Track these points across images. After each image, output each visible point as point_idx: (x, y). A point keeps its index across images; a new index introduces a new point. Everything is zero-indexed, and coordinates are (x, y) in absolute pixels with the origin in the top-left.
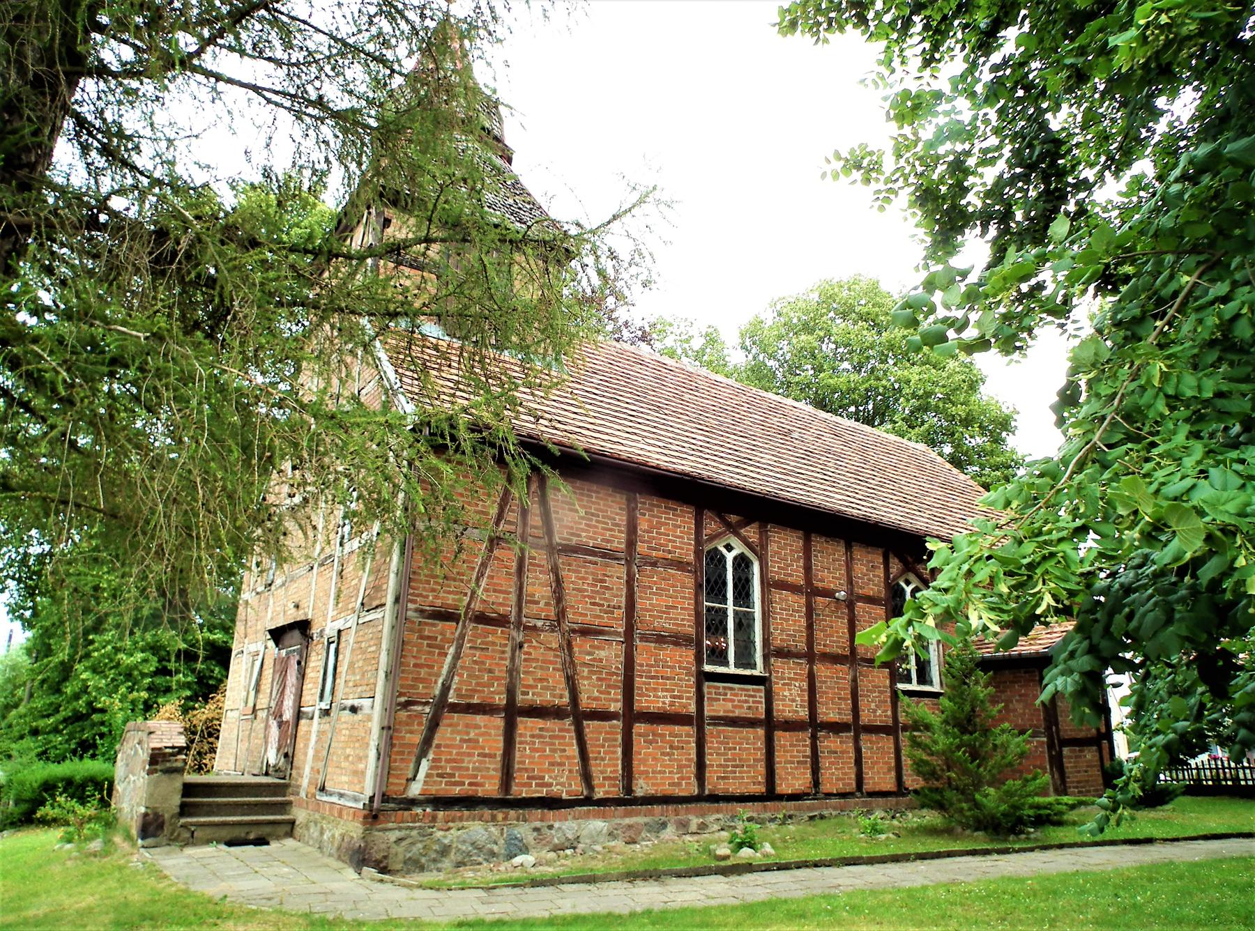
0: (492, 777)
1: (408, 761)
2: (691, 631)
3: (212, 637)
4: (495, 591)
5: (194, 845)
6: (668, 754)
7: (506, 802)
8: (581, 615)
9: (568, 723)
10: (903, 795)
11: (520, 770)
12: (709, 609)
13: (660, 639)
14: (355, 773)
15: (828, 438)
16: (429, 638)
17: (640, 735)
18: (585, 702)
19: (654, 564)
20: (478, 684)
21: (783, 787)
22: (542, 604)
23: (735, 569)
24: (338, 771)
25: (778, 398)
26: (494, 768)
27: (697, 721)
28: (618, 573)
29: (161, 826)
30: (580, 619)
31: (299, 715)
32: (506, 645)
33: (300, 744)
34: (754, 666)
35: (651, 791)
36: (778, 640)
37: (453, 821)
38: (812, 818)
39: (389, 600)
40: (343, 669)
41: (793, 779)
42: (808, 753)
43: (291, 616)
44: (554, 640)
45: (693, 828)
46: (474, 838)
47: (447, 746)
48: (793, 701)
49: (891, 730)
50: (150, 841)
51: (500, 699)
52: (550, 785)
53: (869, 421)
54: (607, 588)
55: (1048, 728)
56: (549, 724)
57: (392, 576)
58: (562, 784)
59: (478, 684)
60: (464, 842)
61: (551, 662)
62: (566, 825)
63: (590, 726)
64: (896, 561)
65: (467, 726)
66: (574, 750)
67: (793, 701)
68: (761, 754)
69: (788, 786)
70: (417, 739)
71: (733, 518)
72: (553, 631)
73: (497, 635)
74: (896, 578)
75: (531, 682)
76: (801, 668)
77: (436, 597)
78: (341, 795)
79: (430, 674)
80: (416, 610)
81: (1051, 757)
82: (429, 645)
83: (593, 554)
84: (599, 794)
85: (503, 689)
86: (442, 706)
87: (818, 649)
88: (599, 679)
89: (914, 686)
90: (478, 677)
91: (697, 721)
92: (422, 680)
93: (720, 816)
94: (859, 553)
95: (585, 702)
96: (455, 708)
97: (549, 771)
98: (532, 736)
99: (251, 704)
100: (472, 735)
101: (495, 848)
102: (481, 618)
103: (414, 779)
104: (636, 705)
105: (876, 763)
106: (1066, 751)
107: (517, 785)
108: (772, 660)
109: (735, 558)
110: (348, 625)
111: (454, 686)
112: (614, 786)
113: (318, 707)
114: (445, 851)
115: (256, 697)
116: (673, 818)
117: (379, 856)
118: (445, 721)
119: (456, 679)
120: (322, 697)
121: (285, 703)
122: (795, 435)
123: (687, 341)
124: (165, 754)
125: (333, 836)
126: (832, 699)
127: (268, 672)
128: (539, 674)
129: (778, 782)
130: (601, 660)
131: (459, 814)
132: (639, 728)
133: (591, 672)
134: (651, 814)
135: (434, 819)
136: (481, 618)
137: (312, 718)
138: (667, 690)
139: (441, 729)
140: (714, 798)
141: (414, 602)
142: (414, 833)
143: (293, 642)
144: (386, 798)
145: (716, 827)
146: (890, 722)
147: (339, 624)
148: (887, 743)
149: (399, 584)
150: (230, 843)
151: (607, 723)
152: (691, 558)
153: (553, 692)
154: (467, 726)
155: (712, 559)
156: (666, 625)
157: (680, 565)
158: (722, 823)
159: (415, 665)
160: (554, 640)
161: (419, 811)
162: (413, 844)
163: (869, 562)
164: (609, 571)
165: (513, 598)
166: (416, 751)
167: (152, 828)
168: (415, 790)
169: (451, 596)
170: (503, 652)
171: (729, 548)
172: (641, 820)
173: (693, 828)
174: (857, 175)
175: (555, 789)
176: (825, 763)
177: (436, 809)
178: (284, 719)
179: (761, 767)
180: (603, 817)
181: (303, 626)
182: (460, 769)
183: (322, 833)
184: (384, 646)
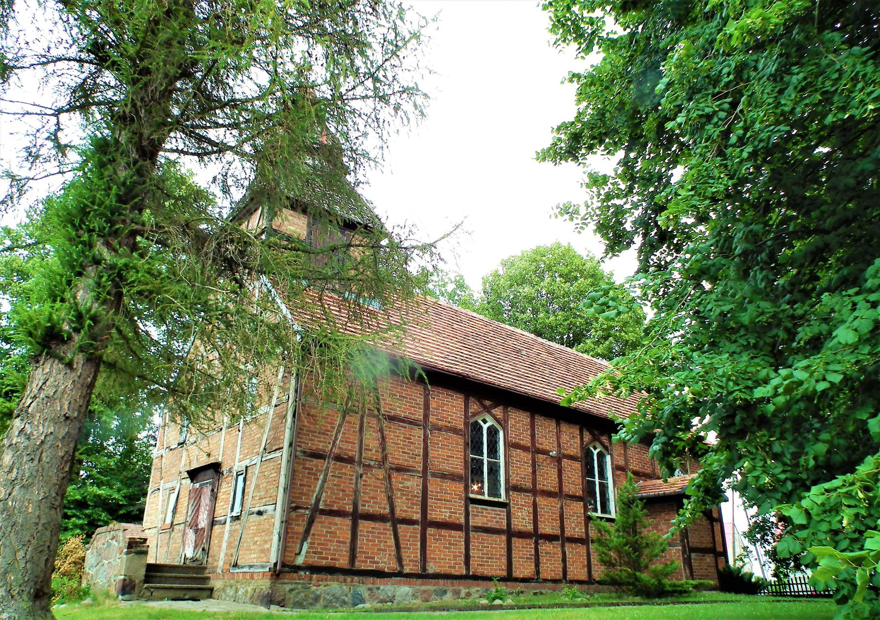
0: (344, 556)
1: (296, 543)
2: (462, 472)
3: (100, 492)
4: (347, 442)
5: (152, 600)
6: (447, 548)
7: (351, 572)
8: (397, 459)
9: (388, 524)
10: (592, 584)
11: (360, 552)
12: (473, 459)
13: (443, 476)
14: (263, 551)
15: (544, 355)
16: (309, 469)
17: (431, 535)
18: (399, 513)
19: (440, 429)
20: (336, 498)
21: (517, 573)
22: (374, 451)
23: (488, 435)
24: (248, 552)
25: (512, 328)
26: (345, 550)
27: (465, 528)
28: (418, 433)
29: (133, 588)
30: (396, 461)
31: (213, 523)
32: (352, 475)
33: (214, 541)
34: (499, 496)
35: (438, 570)
36: (513, 481)
37: (322, 581)
38: (535, 594)
39: (286, 445)
40: (250, 489)
41: (524, 568)
42: (533, 553)
43: (204, 461)
44: (381, 473)
45: (463, 595)
46: (334, 592)
47: (318, 535)
48: (524, 519)
49: (584, 541)
50: (127, 597)
51: (349, 508)
52: (378, 563)
53: (571, 345)
54: (412, 443)
55: (682, 541)
56: (377, 525)
57: (288, 431)
58: (385, 563)
59: (336, 498)
60: (328, 594)
61: (378, 487)
62: (387, 588)
63: (401, 528)
64: (588, 433)
65: (330, 523)
66: (392, 542)
67: (524, 519)
68: (504, 552)
69: (521, 572)
70: (301, 529)
71: (488, 403)
72: (380, 468)
73: (347, 469)
74: (588, 444)
75: (367, 499)
76: (529, 498)
77: (312, 444)
78: (251, 567)
79: (309, 491)
80: (301, 451)
81: (684, 559)
82: (309, 473)
83: (403, 421)
84: (407, 570)
85: (351, 502)
86: (317, 511)
87: (539, 487)
88: (407, 499)
89: (599, 514)
90: (337, 494)
91: (465, 528)
92: (305, 494)
93: (479, 589)
94: (564, 427)
95: (399, 513)
96: (323, 512)
97: (377, 554)
98: (368, 532)
99: (168, 521)
100: (333, 529)
101: (346, 599)
102: (339, 458)
103: (299, 554)
104: (429, 516)
105: (576, 562)
106: (693, 555)
107: (359, 561)
108: (511, 493)
109: (488, 428)
110: (253, 463)
111: (323, 499)
112: (416, 566)
113: (229, 515)
114: (317, 599)
115: (173, 517)
116: (451, 588)
117: (280, 599)
118: (317, 520)
119: (324, 494)
120: (232, 510)
121: (201, 517)
122: (524, 353)
123: (444, 286)
124: (137, 542)
125: (247, 591)
126: (548, 519)
127: (184, 501)
128: (372, 494)
129: (514, 569)
130: (408, 488)
131: (325, 577)
132: (430, 531)
133: (402, 495)
134: (437, 584)
135: (311, 579)
136: (339, 458)
137: (225, 523)
138: (447, 508)
139: (315, 524)
140: (476, 578)
141: (300, 446)
142: (300, 586)
143: (206, 477)
144: (284, 565)
145: (476, 595)
146: (584, 536)
147: (247, 462)
148: (582, 549)
149: (292, 435)
150: (173, 600)
151: (412, 527)
152: (462, 427)
153: (381, 507)
154: (330, 523)
155: (474, 428)
156: (447, 467)
157: (455, 431)
158: (480, 593)
159: (301, 485)
160: (381, 473)
161: (302, 573)
162: (299, 593)
163: (571, 433)
164: (414, 433)
165: (357, 446)
166: (301, 537)
167: (128, 589)
168: (300, 560)
169: (321, 444)
170: (351, 480)
171: (485, 421)
172: (431, 588)
173: (463, 595)
174: (567, 217)
175: (381, 565)
176: (543, 559)
177: (312, 573)
178: (200, 527)
179: (504, 560)
180: (410, 584)
181: (215, 468)
182: (326, 549)
183: (237, 591)
184: (283, 472)
